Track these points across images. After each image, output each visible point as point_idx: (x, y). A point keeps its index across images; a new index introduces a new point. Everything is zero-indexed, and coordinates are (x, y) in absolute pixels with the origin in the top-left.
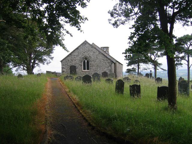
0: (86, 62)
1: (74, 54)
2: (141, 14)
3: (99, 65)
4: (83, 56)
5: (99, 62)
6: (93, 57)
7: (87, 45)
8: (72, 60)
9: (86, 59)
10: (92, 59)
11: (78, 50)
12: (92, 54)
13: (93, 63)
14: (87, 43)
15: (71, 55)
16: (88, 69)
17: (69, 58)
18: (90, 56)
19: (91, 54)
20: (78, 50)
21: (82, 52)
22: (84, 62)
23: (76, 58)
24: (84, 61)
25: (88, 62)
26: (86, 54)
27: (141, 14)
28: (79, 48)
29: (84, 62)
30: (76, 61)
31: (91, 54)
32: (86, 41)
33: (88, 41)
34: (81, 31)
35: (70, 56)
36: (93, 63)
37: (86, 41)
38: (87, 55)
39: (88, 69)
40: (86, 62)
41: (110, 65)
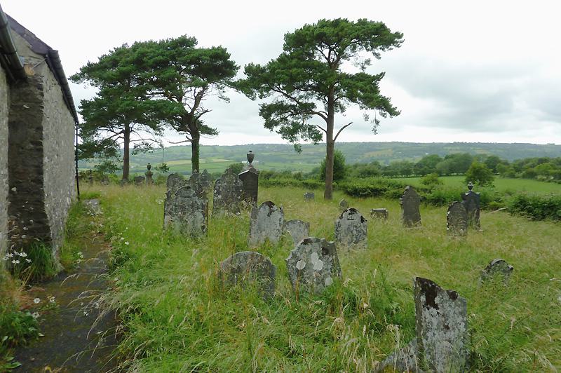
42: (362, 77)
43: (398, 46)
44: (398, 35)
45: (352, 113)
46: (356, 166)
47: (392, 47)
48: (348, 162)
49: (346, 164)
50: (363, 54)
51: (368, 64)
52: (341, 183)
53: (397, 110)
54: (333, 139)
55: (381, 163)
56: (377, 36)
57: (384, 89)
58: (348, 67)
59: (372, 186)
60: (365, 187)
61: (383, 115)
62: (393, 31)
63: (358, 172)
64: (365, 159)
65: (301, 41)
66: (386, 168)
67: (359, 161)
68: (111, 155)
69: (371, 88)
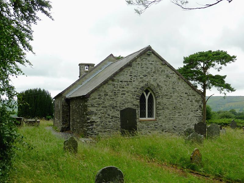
0: (147, 98)
1: (121, 78)
2: (206, 75)
3: (178, 105)
4: (142, 85)
5: (179, 99)
6: (164, 88)
7: (153, 58)
8: (115, 94)
9: (147, 92)
10: (163, 90)
11: (131, 70)
12: (163, 80)
13: (165, 100)
14: (154, 52)
15: (113, 80)
16: (150, 115)
17: (108, 88)
18: (158, 86)
19: (162, 78)
20: (131, 70)
21: (139, 74)
22: (142, 98)
23: (126, 89)
24: (143, 95)
25: (151, 98)
26: (151, 81)
27: (206, 75)
28: (134, 63)
29: (142, 98)
30: (124, 96)
31: (162, 78)
32: (149, 49)
33: (153, 48)
34: (167, 82)
35: (110, 82)
36: (165, 100)
37: (149, 49)
38: (152, 82)
39: (150, 115)
40: (147, 98)
41: (200, 106)
42: (218, 77)
43: (234, 62)
44: (234, 57)
45: (213, 92)
46: (219, 113)
47: (231, 62)
48: (214, 109)
49: (212, 111)
50: (218, 65)
51: (221, 69)
52: (210, 121)
53: (234, 89)
54: (206, 100)
55: (237, 111)
56: (224, 58)
57: (227, 81)
58: (212, 71)
59: (224, 122)
60: (221, 122)
61: (228, 91)
62: (231, 56)
63: (220, 116)
64: (225, 108)
65: (191, 61)
66: (240, 114)
67: (222, 109)
68: (84, 113)
69: (221, 82)
